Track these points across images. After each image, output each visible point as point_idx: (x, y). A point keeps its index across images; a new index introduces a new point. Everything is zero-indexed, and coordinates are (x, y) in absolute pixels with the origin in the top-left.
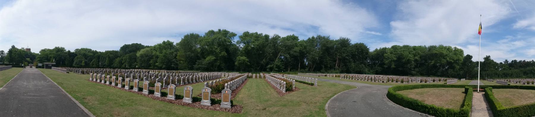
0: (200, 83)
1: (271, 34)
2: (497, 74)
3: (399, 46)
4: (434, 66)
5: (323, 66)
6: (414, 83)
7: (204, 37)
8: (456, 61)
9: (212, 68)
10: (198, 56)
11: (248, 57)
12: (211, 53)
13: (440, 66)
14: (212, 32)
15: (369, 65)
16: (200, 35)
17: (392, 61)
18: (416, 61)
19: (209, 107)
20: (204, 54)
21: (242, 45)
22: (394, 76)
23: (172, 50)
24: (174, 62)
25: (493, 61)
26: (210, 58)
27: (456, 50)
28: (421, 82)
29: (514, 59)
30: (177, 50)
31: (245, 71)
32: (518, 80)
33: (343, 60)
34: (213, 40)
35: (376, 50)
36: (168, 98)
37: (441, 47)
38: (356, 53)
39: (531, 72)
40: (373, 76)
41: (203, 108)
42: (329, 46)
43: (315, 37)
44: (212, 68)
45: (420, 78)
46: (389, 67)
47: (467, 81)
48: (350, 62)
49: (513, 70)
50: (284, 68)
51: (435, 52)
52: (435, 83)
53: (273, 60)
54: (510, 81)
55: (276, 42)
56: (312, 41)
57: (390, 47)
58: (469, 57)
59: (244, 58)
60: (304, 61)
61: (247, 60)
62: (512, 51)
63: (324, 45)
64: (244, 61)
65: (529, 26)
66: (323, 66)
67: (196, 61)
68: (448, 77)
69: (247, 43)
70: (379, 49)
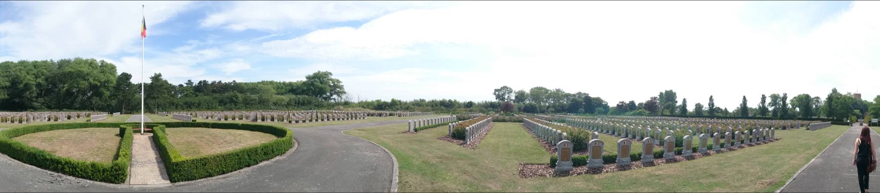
2: (173, 104)
3: (12, 63)
4: (69, 93)
6: (38, 123)
8: (105, 84)
13: (78, 92)
18: (39, 85)
22: (8, 113)
25: (166, 82)
27: (104, 65)
28: (49, 120)
32: (209, 113)
37: (79, 62)
45: (46, 114)
47: (123, 115)
49: (202, 97)
51: (67, 69)
52: (72, 121)
54: (196, 116)
58: (126, 77)
62: (199, 65)
65: (227, 24)
68: (92, 109)
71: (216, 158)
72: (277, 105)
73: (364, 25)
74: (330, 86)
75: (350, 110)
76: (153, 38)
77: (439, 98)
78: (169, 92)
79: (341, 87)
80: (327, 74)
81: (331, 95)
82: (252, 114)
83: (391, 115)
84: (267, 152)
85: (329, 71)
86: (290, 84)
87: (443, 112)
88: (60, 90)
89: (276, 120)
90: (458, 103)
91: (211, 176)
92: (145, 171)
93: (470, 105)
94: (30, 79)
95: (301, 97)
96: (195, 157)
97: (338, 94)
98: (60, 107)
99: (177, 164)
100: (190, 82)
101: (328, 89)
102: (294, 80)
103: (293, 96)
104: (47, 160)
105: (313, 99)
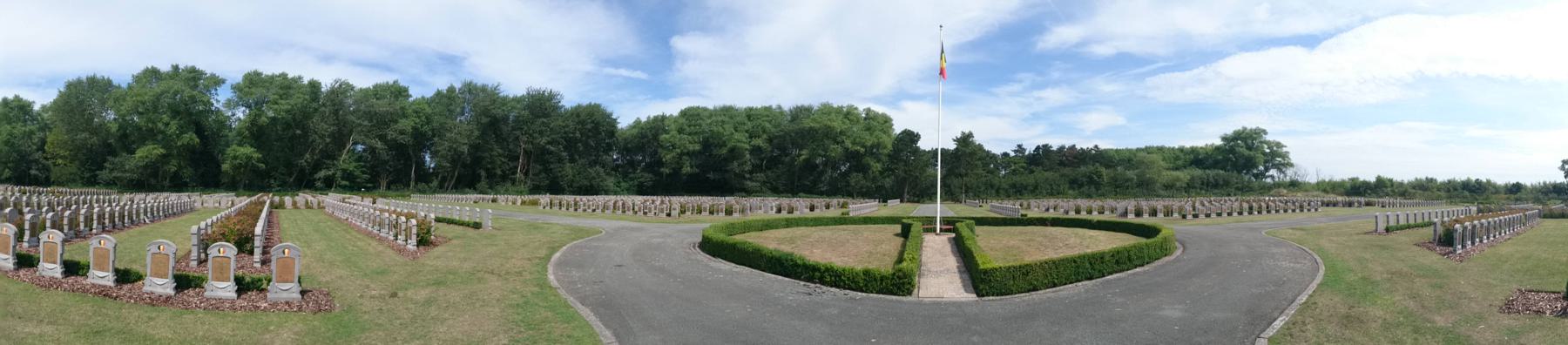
0: (144, 228)
1: (327, 80)
2: (992, 186)
3: (705, 109)
4: (809, 166)
5: (483, 173)
6: (759, 215)
7: (130, 87)
8: (873, 151)
9: (153, 181)
10: (110, 145)
11: (259, 148)
12: (149, 135)
13: (825, 164)
14: (152, 74)
15: (616, 168)
16: (115, 83)
17: (682, 154)
18: (756, 150)
19: (233, 301)
20: (127, 139)
21: (241, 113)
22: (704, 199)
23: (30, 127)
24: (36, 161)
25: (980, 147)
26: (148, 151)
27: (870, 116)
28: (779, 211)
29: (1041, 143)
30: (45, 127)
31: (251, 188)
32: (1052, 202)
33: (540, 157)
34: (158, 97)
35: (638, 122)
36: (89, 281)
37: (827, 110)
38: (578, 135)
39: (1091, 181)
40: (630, 199)
41: (217, 306)
42: (499, 112)
43: (458, 86)
44: (153, 181)
45: (773, 202)
46: (676, 172)
47: (905, 205)
48: (560, 160)
49: (1040, 175)
50: (368, 181)
51: (808, 123)
52: (817, 213)
53: (334, 158)
54: (1029, 207)
55: (341, 103)
56: (446, 99)
57: (676, 113)
58: (910, 138)
59: (247, 150)
60: (424, 162)
61: (256, 155)
62: (1036, 117)
63: (486, 112)
64: (249, 158)
65: (1084, 43)
66: (483, 173)
67: (105, 161)
68: (851, 195)
69: (256, 106)
70: (644, 119)
71: (1042, 265)
72: (1170, 188)
73: (1325, 43)
74: (1264, 154)
75: (1300, 196)
76: (952, 72)
77: (1460, 176)
78: (986, 165)
79: (1285, 156)
80: (1259, 133)
81: (1267, 169)
82: (1121, 204)
83: (1368, 204)
84: (1121, 261)
85: (1262, 127)
86: (1193, 150)
87: (1464, 200)
88: (793, 160)
89: (1161, 215)
90: (1494, 186)
91: (1035, 289)
92: (940, 280)
93: (1516, 189)
94: (741, 140)
95: (1211, 173)
96: (1017, 264)
97: (1279, 167)
98: (793, 190)
99: (985, 272)
100: (1020, 149)
101: (1261, 158)
102: (1200, 143)
103: (1198, 172)
104: (797, 265)
105: (1234, 177)
